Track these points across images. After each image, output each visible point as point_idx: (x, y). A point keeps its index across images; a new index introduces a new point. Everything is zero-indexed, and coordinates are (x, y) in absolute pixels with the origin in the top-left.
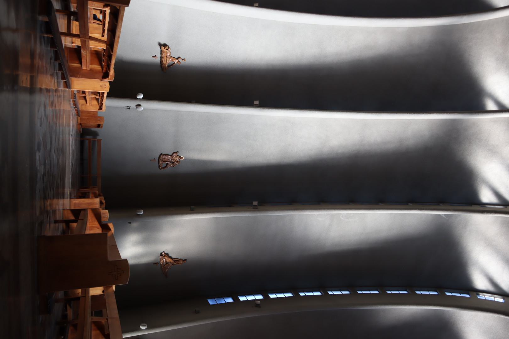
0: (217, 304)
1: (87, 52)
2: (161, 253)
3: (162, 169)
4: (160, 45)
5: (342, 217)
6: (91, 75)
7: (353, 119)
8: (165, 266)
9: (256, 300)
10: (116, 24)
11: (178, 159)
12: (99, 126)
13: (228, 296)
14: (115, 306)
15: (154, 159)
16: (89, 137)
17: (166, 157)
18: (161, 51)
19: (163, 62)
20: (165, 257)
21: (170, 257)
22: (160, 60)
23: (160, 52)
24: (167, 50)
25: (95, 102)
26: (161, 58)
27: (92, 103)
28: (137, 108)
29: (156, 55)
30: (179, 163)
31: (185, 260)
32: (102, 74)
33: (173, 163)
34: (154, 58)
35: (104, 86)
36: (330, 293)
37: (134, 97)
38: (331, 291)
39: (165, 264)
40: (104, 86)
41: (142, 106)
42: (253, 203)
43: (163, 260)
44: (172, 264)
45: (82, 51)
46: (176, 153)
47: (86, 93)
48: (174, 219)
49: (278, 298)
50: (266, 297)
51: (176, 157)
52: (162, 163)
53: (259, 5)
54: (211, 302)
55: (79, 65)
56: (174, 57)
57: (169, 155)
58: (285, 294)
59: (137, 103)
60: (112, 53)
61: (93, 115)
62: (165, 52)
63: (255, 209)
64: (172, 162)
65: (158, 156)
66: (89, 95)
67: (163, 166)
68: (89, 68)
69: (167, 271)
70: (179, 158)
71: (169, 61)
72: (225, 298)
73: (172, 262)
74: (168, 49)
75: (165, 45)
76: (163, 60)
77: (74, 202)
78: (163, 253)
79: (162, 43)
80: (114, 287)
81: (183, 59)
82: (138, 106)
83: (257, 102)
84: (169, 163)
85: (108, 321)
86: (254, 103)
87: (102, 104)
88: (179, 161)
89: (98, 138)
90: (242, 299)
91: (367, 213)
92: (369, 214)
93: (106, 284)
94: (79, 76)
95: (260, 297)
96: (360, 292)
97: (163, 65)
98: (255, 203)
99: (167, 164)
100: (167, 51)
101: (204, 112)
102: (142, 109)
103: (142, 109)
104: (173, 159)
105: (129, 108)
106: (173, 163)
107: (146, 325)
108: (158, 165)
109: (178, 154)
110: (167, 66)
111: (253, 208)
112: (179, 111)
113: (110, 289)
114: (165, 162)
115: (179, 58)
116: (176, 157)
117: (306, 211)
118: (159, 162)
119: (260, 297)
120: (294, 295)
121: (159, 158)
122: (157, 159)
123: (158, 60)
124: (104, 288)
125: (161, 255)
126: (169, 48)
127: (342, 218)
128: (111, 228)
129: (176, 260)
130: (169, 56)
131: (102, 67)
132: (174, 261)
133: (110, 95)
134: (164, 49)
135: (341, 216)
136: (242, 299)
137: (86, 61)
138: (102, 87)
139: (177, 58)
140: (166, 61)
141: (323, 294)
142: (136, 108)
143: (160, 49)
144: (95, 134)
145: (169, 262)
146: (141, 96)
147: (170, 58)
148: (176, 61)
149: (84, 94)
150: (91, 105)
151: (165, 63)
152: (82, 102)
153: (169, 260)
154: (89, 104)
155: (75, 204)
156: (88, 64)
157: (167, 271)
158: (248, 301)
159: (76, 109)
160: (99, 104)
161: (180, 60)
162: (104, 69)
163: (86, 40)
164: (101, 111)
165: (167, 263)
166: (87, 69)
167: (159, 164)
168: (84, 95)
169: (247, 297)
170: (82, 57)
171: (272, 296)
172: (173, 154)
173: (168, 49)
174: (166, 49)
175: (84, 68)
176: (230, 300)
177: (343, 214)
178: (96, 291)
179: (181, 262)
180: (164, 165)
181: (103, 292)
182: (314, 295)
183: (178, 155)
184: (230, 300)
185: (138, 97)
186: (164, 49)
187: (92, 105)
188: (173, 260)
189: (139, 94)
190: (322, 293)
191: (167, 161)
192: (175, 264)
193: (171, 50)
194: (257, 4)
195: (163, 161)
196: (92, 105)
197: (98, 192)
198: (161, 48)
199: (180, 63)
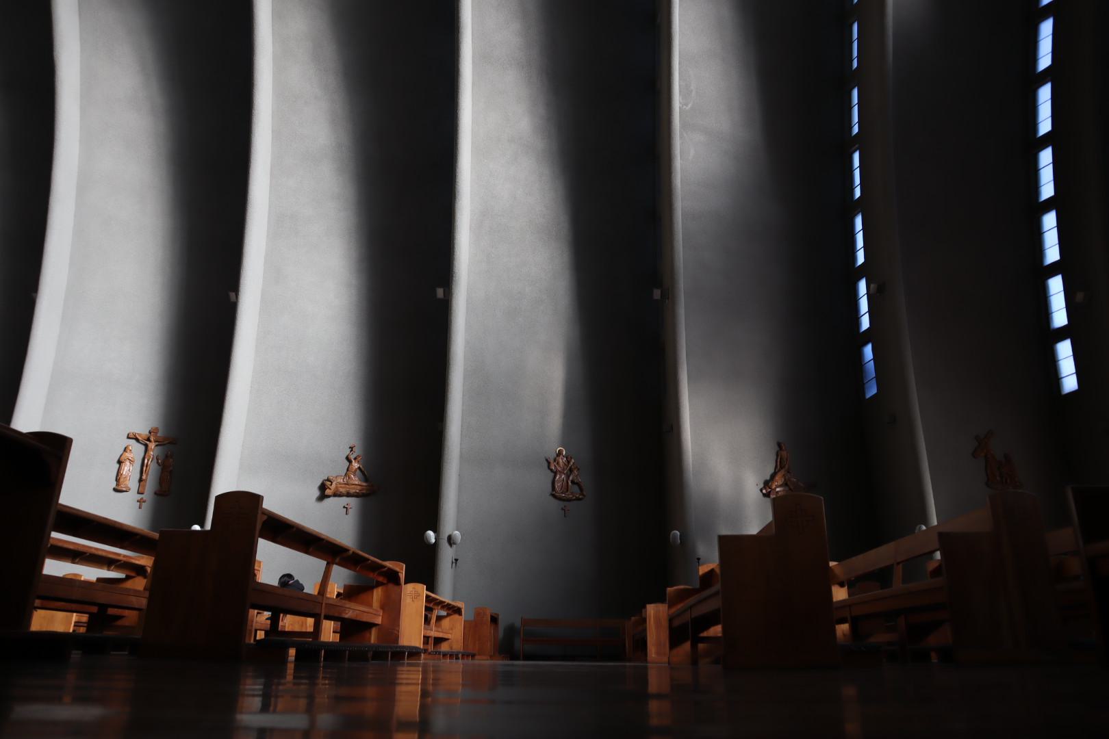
0: (877, 377)
1: (347, 606)
2: (764, 495)
3: (585, 493)
4: (322, 497)
5: (686, 105)
6: (393, 608)
7: (473, 84)
8: (792, 488)
9: (868, 293)
10: (295, 529)
11: (562, 461)
12: (494, 620)
13: (860, 355)
14: (872, 554)
15: (562, 509)
16: (518, 644)
17: (558, 485)
18: (335, 495)
19: (358, 491)
20: (774, 487)
21: (773, 476)
22: (353, 498)
23: (336, 498)
24: (332, 482)
25: (446, 623)
26: (348, 495)
27: (448, 628)
28: (454, 544)
29: (344, 507)
30: (571, 458)
31: (779, 445)
32: (391, 586)
33: (571, 470)
34: (350, 511)
35: (413, 596)
36: (856, 130)
37: (434, 548)
38: (851, 128)
39: (787, 488)
40: (413, 596)
41: (451, 533)
42: (657, 300)
43: (777, 492)
44: (788, 472)
45: (346, 616)
46: (549, 463)
47: (428, 635)
48: (691, 469)
49: (865, 247)
50: (862, 271)
51: (558, 463)
52: (572, 493)
53: (234, 291)
54: (872, 391)
55: (374, 631)
56: (348, 470)
57: (555, 477)
58: (861, 295)
59: (444, 544)
60: (351, 552)
61: (472, 628)
62: (337, 487)
63: (669, 294)
64: (569, 473)
65: (556, 502)
66: (431, 630)
67: (579, 491)
68: (379, 609)
69: (802, 485)
70: (561, 456)
71: (355, 480)
72: (864, 360)
73: (783, 473)
74: (330, 481)
75: (323, 487)
76: (354, 491)
77: (653, 656)
78: (764, 491)
79: (317, 493)
80: (832, 564)
81: (351, 451)
82: (452, 542)
83: (440, 293)
84: (571, 478)
85: (903, 561)
86: (440, 299)
87: (449, 604)
88: (567, 458)
89: (518, 624)
90: (865, 323)
91: (678, 43)
92: (680, 45)
93: (829, 579)
94: (396, 632)
95: (862, 286)
96: (855, 64)
97: (364, 491)
98: (657, 294)
99: (573, 482)
100: (334, 483)
101: (463, 405)
102: (457, 533)
103: (457, 533)
104: (564, 470)
105: (456, 560)
106: (571, 470)
107: (918, 528)
108: (575, 502)
109: (552, 461)
110: (364, 484)
111: (668, 298)
112: (461, 456)
113: (838, 571)
114: (570, 487)
115: (348, 458)
116: (558, 463)
117: (674, 185)
118: (569, 500)
119: (862, 286)
120: (859, 210)
121: (560, 499)
122: (562, 504)
123: (352, 502)
124: (834, 584)
125: (767, 495)
126: (328, 480)
127: (690, 106)
128: (709, 569)
129: (780, 465)
130: (345, 480)
131: (379, 584)
132: (781, 468)
133: (431, 587)
134: (330, 489)
135: (685, 107)
136: (865, 323)
137: (366, 614)
138: (417, 596)
139: (348, 463)
140: (356, 485)
141: (857, 146)
142: (455, 546)
143: (331, 498)
144: (511, 631)
145: (783, 480)
146: (430, 536)
147: (349, 478)
148: (356, 465)
149: (430, 639)
150: (451, 632)
151: (359, 487)
152: (444, 647)
153: (779, 480)
154: (450, 635)
155: (658, 653)
156: (371, 611)
157: (802, 485)
158: (870, 311)
159: (460, 656)
160: (451, 615)
161: (352, 457)
162: (381, 579)
163: (326, 604)
164: (463, 610)
165: (785, 484)
166: (381, 614)
167: (574, 500)
168: (431, 641)
169: (862, 313)
170: (358, 619)
171: (861, 258)
172: (551, 470)
173: (330, 481)
174: (331, 485)
175: (379, 620)
176: (868, 351)
177: (680, 103)
178: (840, 594)
179: (784, 453)
180: (576, 489)
181: (842, 585)
182: (860, 167)
183: (555, 460)
184: (868, 351)
185: (433, 541)
186: (330, 489)
187: (452, 629)
188: (779, 471)
189: (426, 538)
190: (854, 148)
191: (567, 482)
192: (787, 466)
193: (332, 475)
194: (232, 295)
195: (567, 491)
196: (452, 629)
197: (633, 618)
198: (328, 496)
199: (359, 456)
